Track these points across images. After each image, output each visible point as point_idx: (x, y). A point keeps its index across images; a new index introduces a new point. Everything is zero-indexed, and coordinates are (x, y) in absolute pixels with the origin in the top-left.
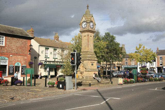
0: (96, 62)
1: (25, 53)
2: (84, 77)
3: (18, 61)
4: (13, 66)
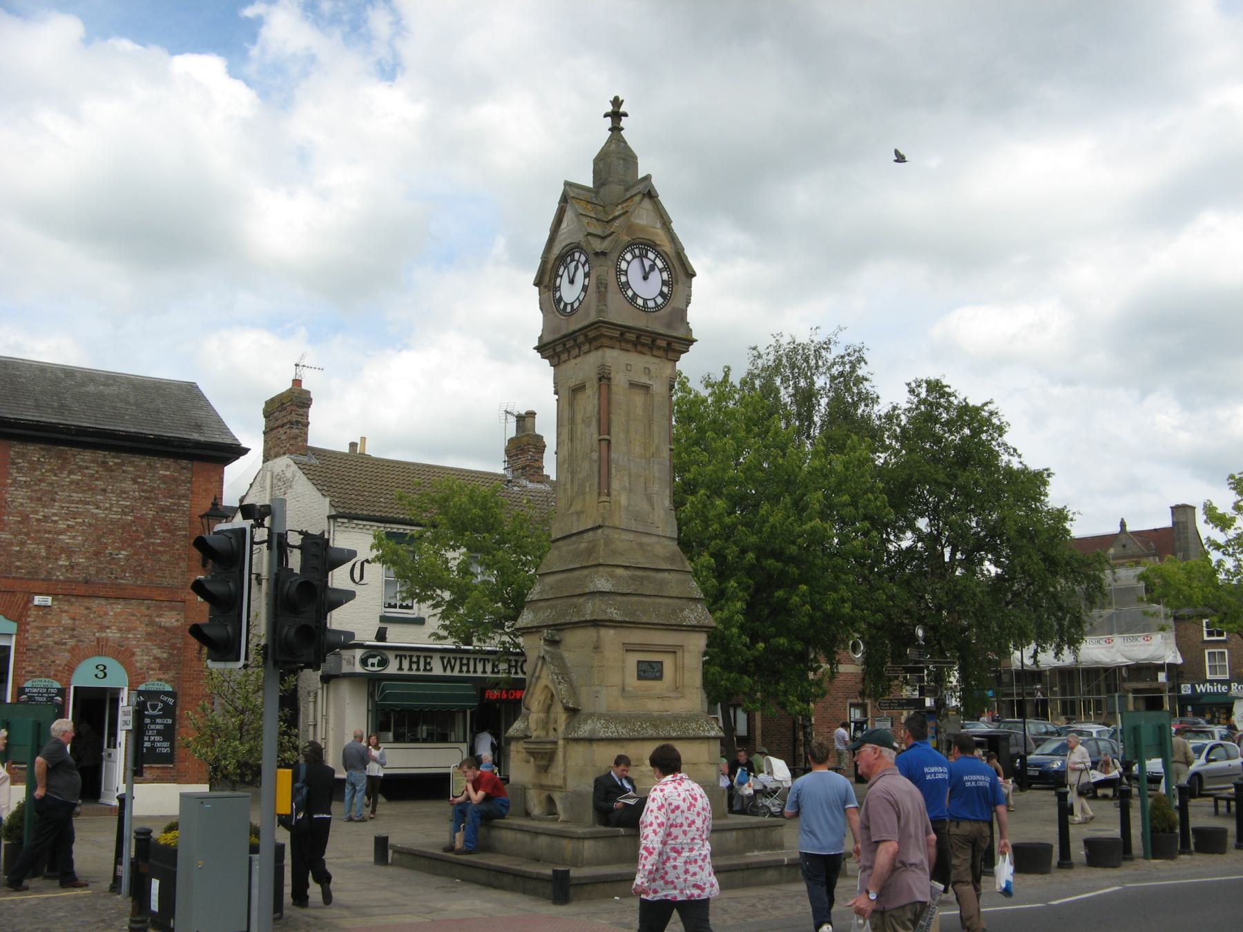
0: (699, 642)
1: (166, 582)
2: (557, 796)
3: (101, 648)
4: (57, 685)
